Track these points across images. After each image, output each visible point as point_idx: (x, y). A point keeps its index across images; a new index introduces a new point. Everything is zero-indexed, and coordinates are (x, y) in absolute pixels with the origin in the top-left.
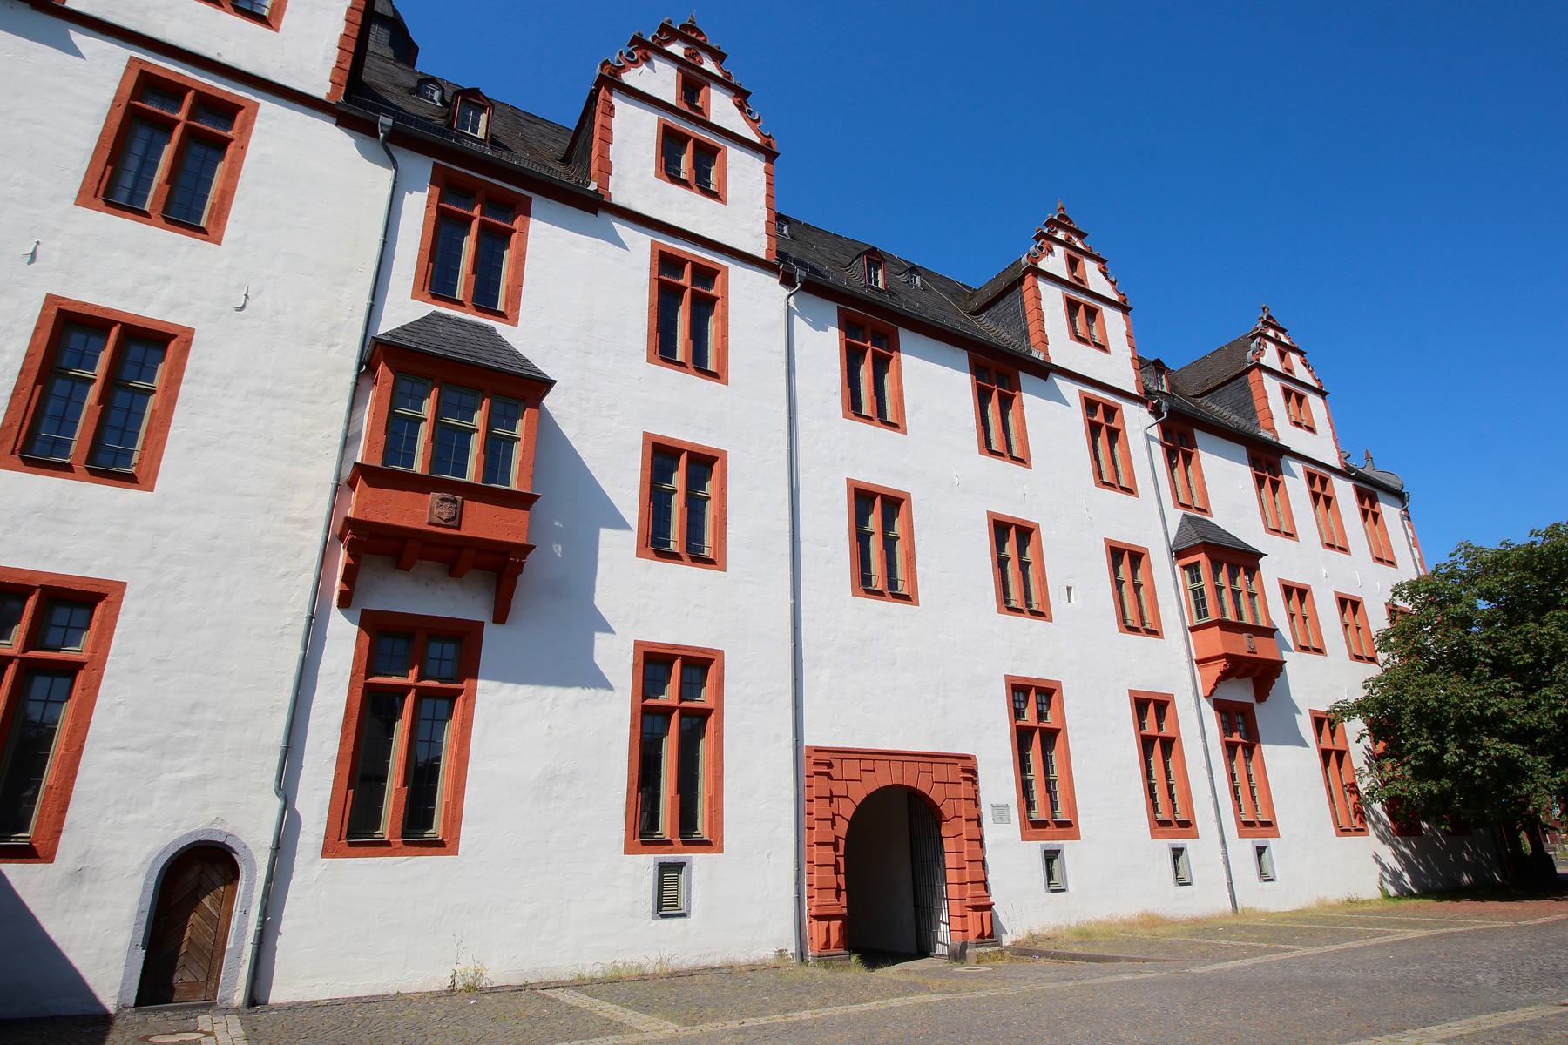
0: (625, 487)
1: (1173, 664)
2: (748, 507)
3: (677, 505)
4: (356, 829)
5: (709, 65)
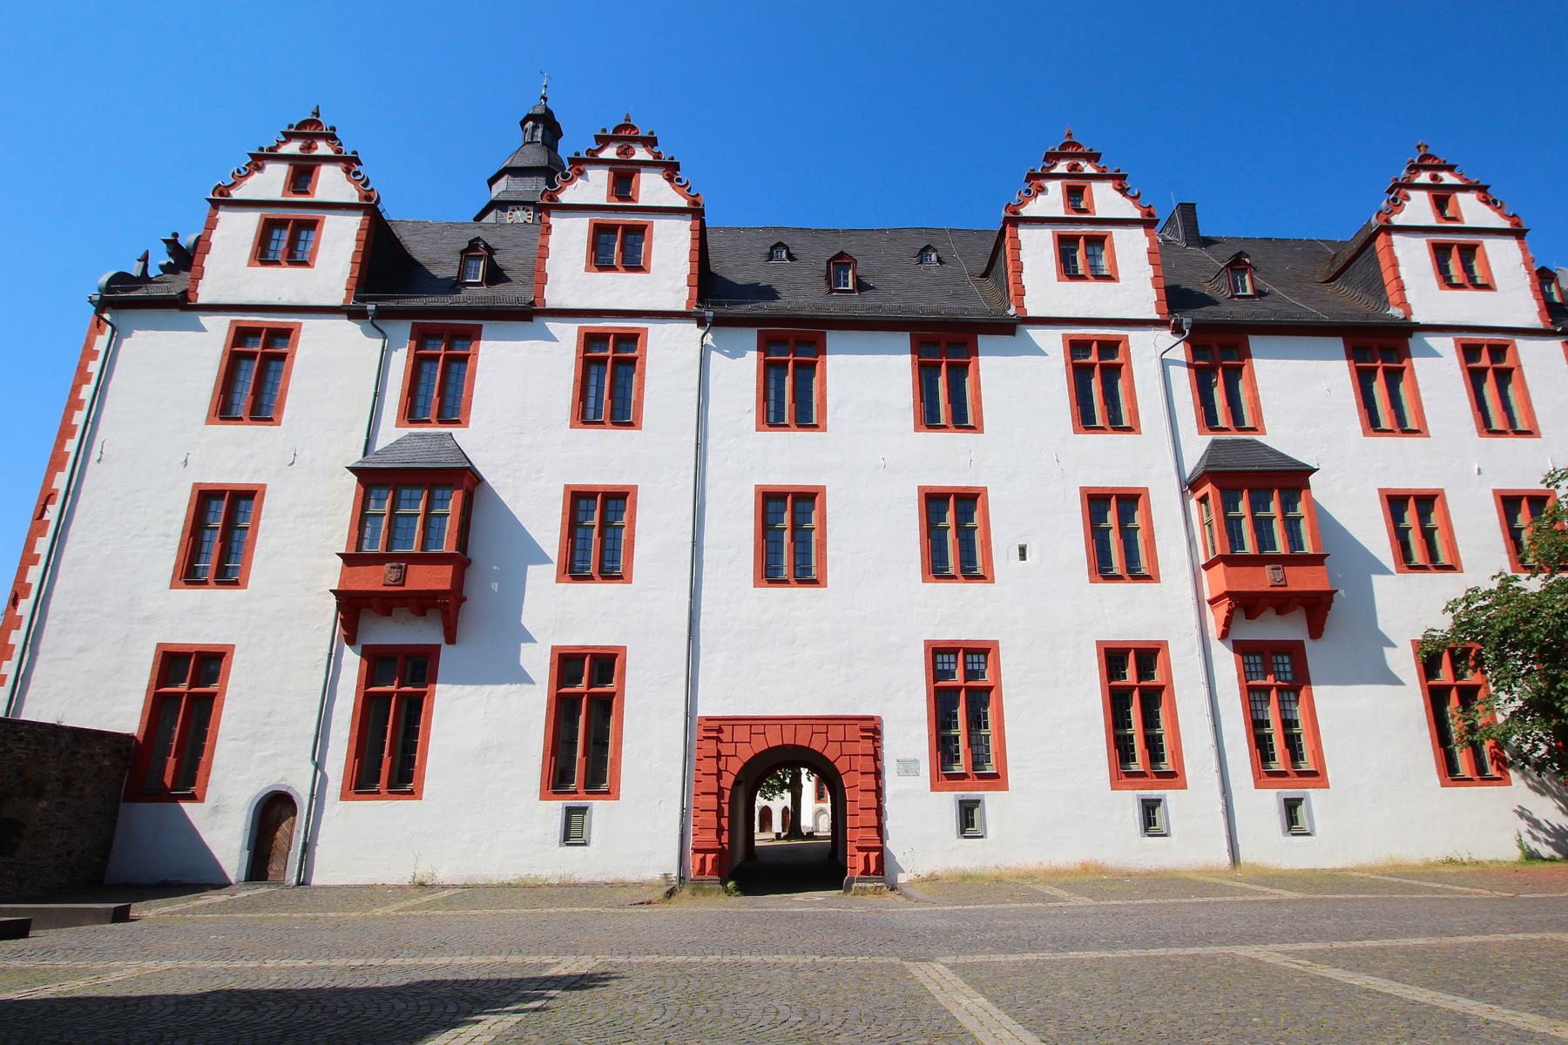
0: (1374, 535)
1: (1171, 607)
2: (655, 534)
3: (1114, 538)
5: (1447, 178)
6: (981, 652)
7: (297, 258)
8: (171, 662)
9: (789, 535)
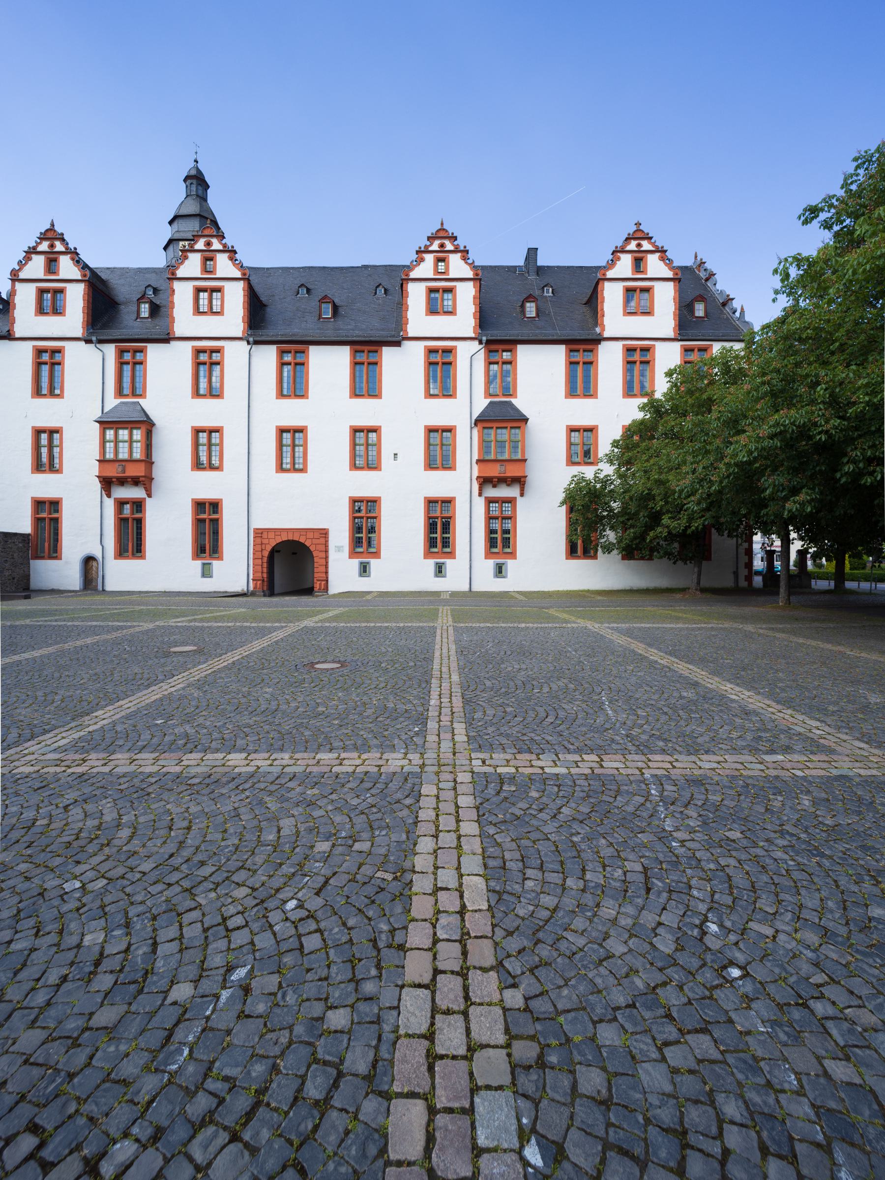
1: (459, 483)
2: (233, 447)
4: (121, 553)
6: (373, 502)
7: (57, 310)
8: (38, 504)
9: (291, 443)
